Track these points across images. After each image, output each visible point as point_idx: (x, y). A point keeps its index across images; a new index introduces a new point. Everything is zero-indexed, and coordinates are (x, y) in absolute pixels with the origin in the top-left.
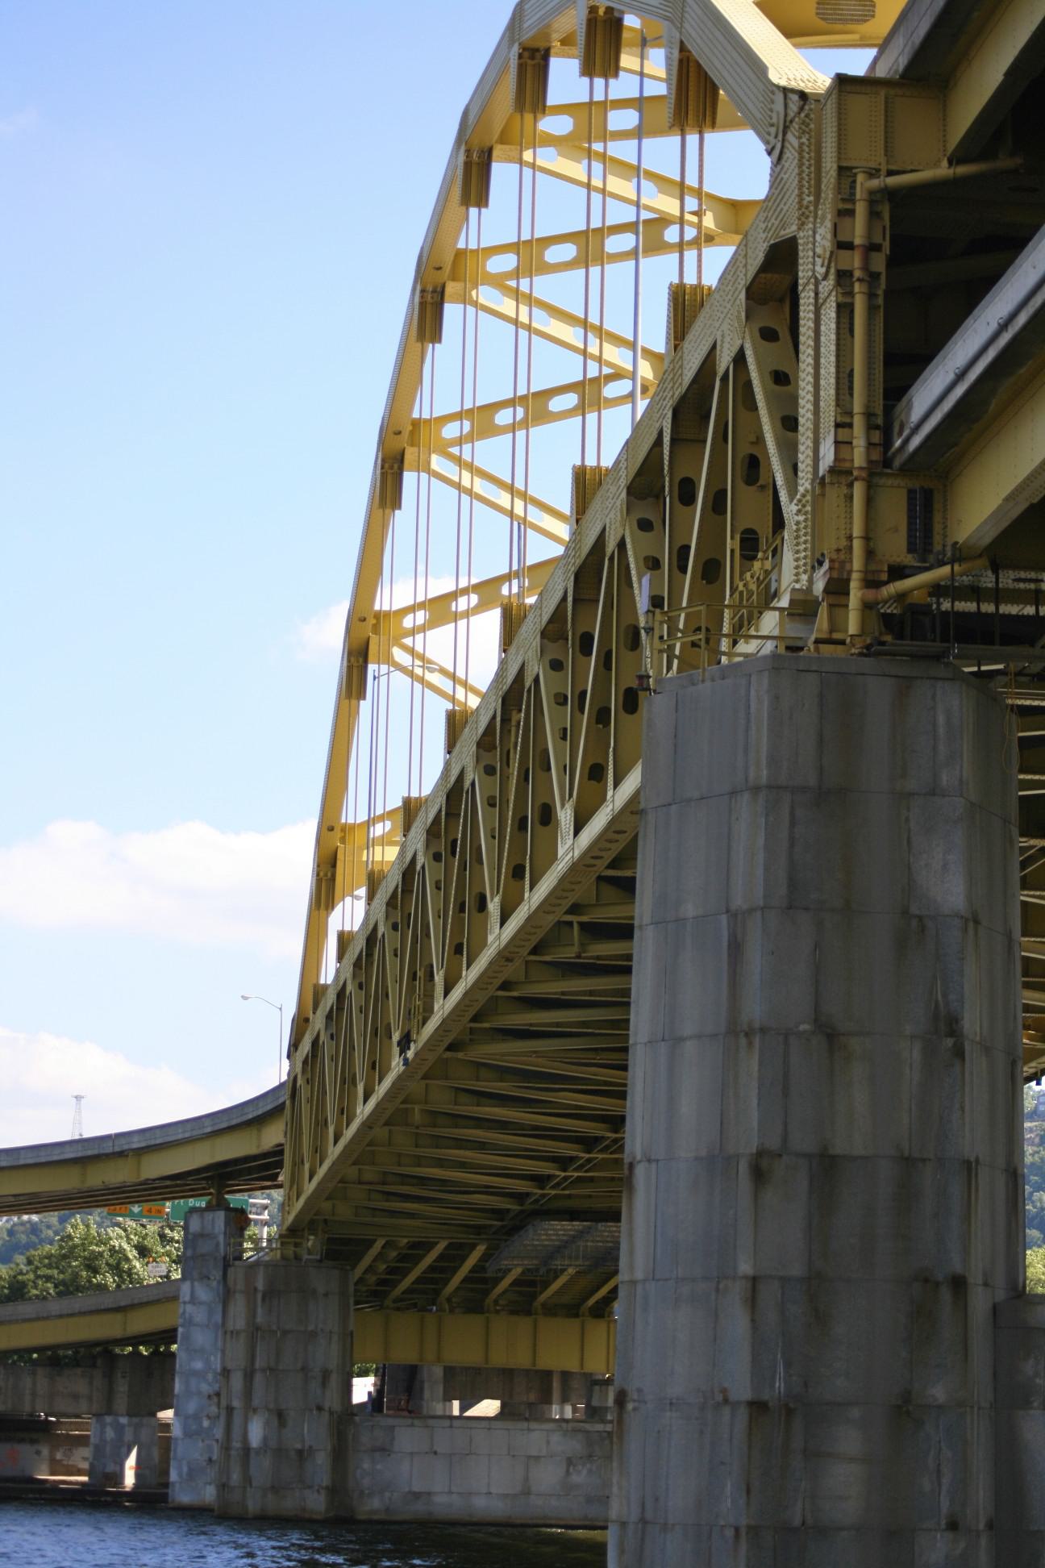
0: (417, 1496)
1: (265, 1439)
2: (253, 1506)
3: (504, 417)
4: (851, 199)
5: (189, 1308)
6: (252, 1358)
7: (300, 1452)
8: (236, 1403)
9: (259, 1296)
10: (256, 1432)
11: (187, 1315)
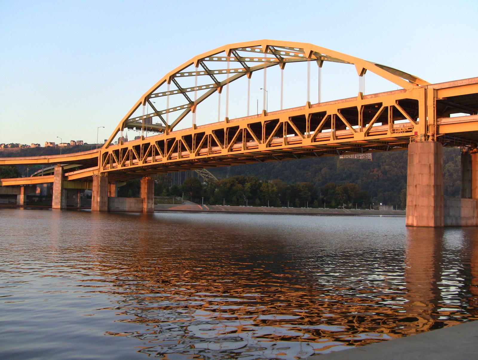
0: (118, 208)
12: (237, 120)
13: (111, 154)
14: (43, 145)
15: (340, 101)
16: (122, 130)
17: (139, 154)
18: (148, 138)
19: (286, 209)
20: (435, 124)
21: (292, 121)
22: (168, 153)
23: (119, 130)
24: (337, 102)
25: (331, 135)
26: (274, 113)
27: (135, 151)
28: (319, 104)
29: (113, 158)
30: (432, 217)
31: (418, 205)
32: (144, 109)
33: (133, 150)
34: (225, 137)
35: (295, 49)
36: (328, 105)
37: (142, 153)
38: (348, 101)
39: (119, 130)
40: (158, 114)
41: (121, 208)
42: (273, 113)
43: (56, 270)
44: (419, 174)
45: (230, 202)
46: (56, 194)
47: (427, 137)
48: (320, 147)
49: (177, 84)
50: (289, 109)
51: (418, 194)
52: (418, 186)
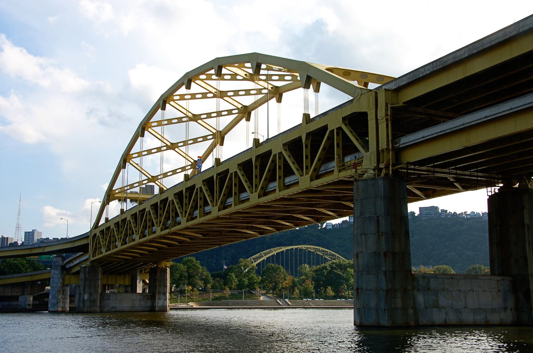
0: (114, 307)
1: (88, 299)
2: (85, 310)
3: (166, 122)
4: (388, 108)
5: (53, 275)
6: (86, 284)
7: (94, 300)
8: (82, 292)
9: (87, 273)
10: (86, 297)
11: (53, 276)
14: (51, 238)
17: (299, 161)
19: (343, 301)
20: (390, 147)
25: (334, 167)
27: (178, 201)
30: (383, 309)
31: (362, 289)
37: (256, 177)
44: (361, 235)
46: (54, 293)
47: (376, 170)
51: (360, 270)
52: (360, 255)
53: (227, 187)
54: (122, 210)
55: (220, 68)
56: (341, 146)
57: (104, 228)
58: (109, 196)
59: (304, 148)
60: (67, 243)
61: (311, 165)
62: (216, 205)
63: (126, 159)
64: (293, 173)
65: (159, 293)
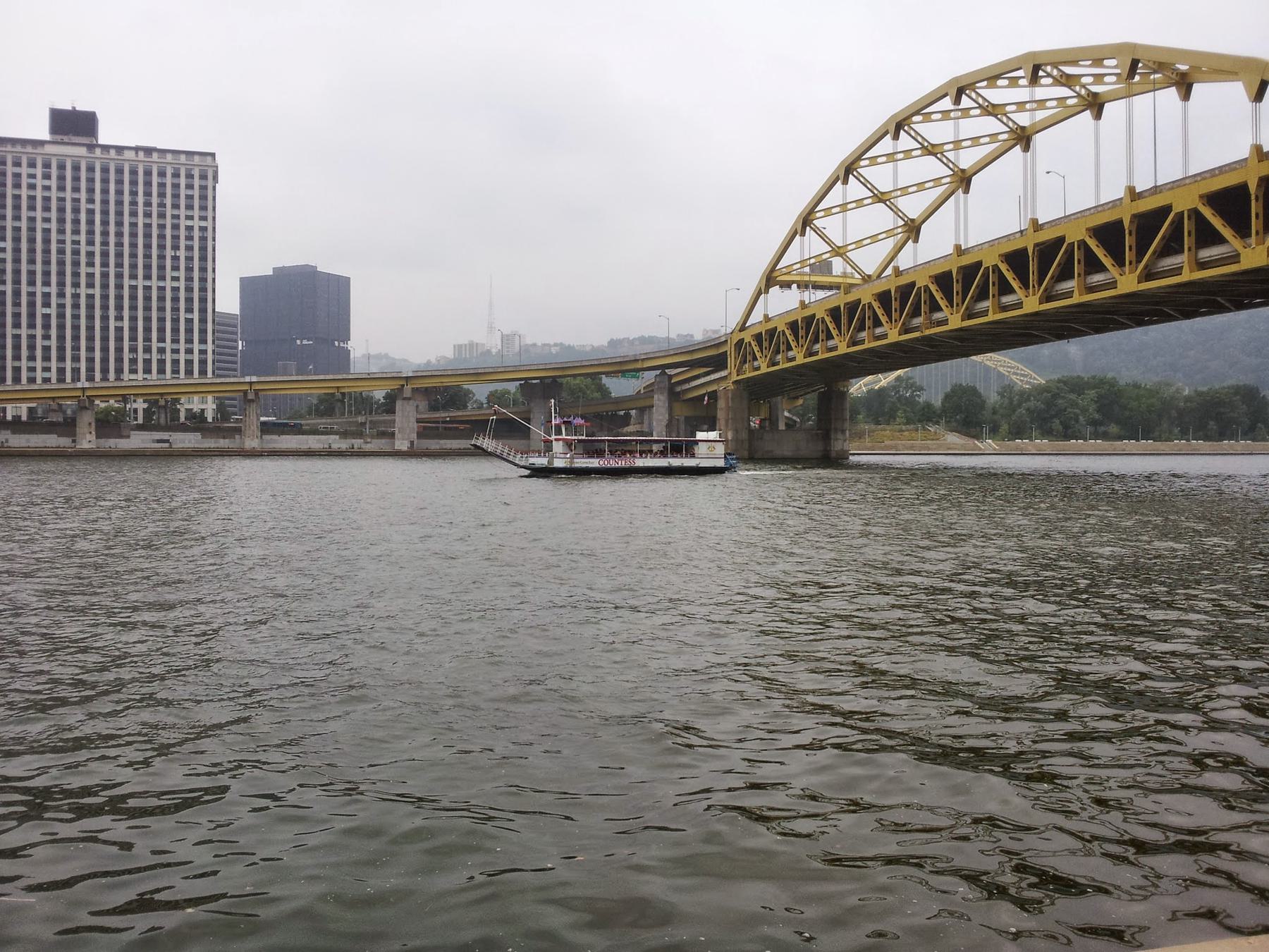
1: (733, 438)
12: (980, 247)
13: (870, 304)
15: (1208, 175)
16: (767, 292)
18: (812, 305)
19: (1184, 444)
21: (1209, 205)
22: (1040, 285)
23: (759, 294)
24: (1199, 178)
26: (1054, 223)
28: (1156, 190)
29: (788, 340)
32: (802, 244)
33: (826, 317)
34: (1129, 241)
35: (1080, 63)
36: (1179, 186)
38: (1226, 172)
39: (759, 294)
40: (838, 251)
41: (658, 445)
42: (1053, 224)
43: (937, 640)
45: (1047, 433)
48: (1238, 281)
49: (865, 183)
50: (1086, 210)
53: (775, 344)
54: (802, 303)
55: (1036, 68)
56: (928, 303)
57: (762, 329)
58: (771, 280)
59: (1127, 236)
60: (681, 353)
61: (963, 303)
62: (844, 341)
63: (806, 221)
64: (940, 309)
65: (836, 430)
